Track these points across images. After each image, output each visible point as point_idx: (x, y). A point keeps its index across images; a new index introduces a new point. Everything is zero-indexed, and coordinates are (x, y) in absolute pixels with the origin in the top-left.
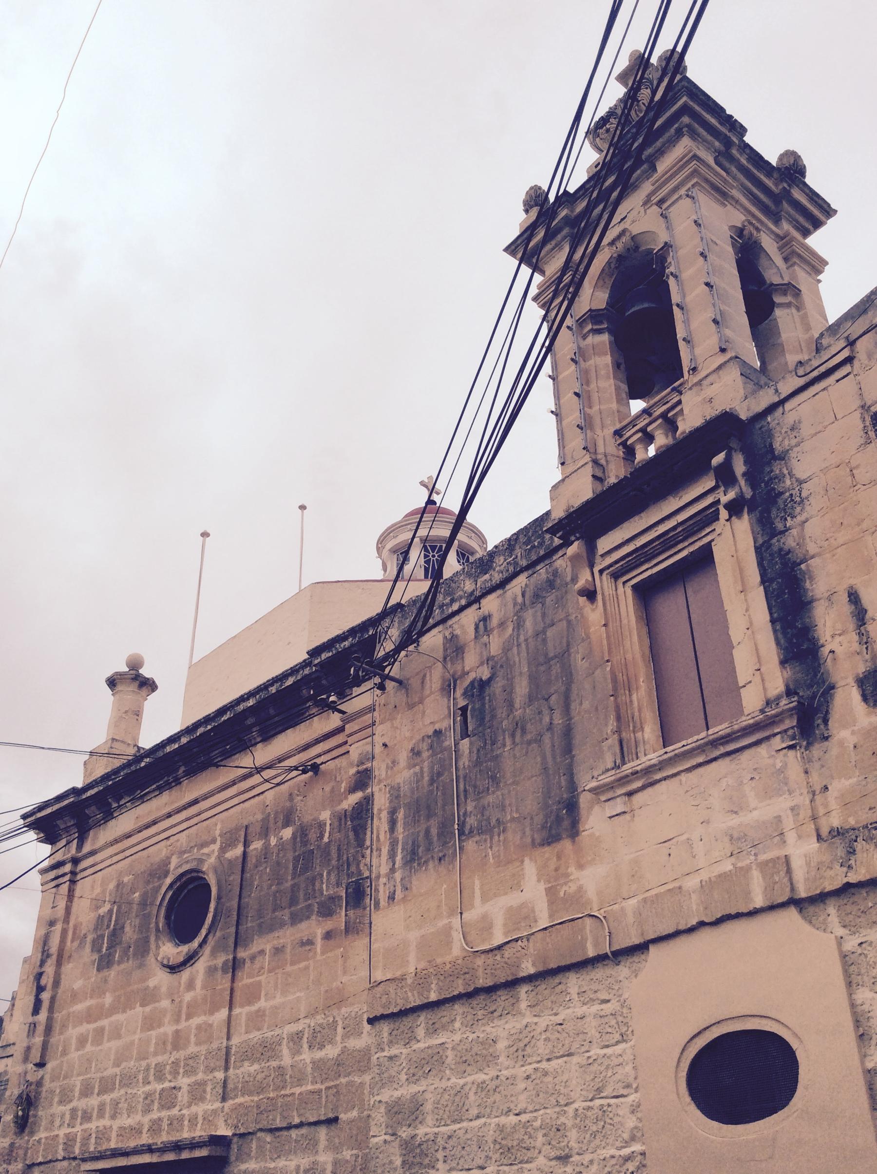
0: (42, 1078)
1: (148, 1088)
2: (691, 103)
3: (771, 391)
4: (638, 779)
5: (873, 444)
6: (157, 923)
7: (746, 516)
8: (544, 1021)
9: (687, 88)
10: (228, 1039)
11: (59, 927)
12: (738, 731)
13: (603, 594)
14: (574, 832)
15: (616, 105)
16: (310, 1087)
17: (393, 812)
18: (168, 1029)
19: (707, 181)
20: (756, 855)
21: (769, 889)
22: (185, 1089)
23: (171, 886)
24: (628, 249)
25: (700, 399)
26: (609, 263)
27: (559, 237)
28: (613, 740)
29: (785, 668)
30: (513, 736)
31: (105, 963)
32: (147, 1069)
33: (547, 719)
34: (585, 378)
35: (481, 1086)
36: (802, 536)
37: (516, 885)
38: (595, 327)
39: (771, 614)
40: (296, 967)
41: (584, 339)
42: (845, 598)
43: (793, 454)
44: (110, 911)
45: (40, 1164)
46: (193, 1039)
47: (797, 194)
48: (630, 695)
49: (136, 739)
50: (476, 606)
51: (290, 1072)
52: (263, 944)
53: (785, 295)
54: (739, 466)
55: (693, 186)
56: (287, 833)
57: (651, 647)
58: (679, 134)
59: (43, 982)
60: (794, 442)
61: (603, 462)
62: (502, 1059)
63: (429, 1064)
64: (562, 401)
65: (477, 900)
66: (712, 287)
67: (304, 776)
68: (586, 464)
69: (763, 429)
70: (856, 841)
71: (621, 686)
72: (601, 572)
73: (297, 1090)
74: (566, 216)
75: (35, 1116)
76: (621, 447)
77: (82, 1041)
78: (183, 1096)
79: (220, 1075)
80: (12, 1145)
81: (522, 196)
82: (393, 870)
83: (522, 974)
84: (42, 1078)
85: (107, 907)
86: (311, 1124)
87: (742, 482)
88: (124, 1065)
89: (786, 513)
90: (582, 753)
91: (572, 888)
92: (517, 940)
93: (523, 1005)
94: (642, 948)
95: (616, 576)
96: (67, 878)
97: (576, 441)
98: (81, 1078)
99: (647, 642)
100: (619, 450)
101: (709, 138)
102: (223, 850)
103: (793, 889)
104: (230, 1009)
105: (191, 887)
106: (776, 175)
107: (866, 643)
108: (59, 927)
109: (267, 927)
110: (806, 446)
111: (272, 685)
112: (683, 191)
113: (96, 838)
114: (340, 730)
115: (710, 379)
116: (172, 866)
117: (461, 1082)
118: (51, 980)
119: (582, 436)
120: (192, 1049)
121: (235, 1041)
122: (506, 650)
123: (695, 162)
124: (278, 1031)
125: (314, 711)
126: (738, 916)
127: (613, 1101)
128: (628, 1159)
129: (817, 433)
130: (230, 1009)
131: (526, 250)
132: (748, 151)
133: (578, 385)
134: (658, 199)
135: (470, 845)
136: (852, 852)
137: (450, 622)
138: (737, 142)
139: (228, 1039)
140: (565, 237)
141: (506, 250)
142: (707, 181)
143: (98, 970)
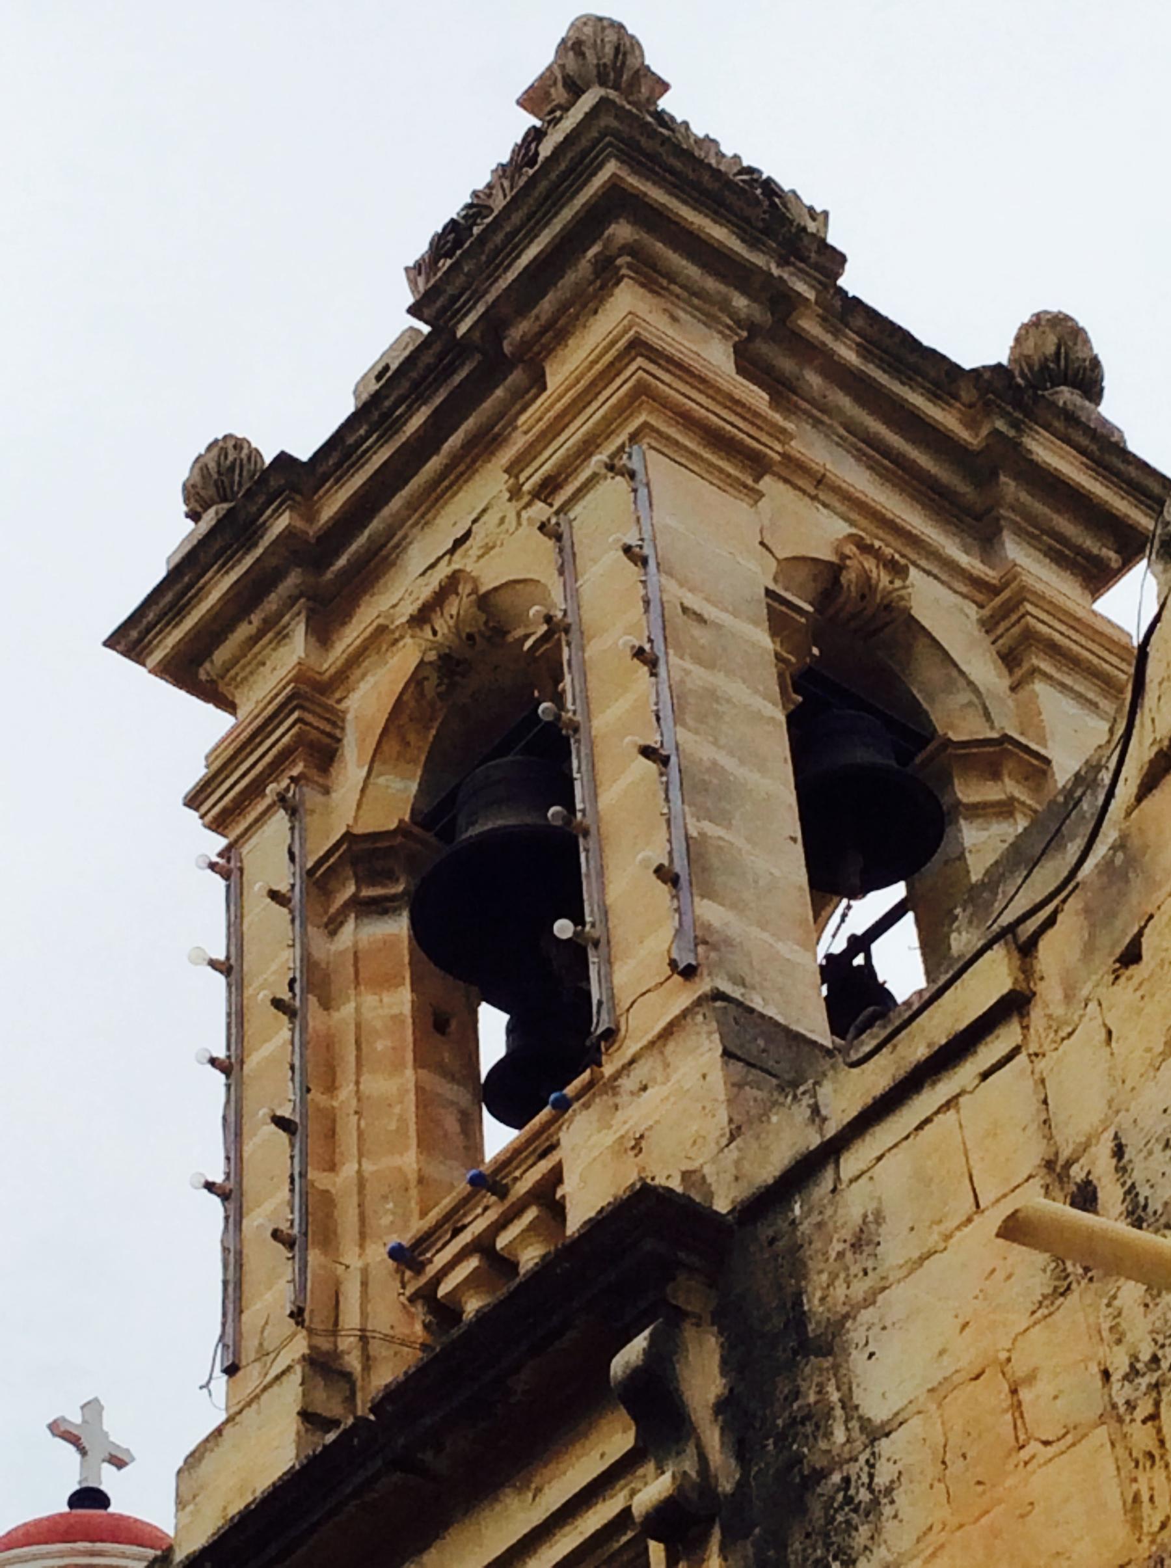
2: (633, 180)
3: (802, 1112)
5: (1073, 1298)
9: (615, 134)
15: (490, 186)
19: (687, 420)
24: (470, 637)
25: (608, 1138)
26: (416, 680)
27: (272, 602)
34: (317, 1067)
38: (368, 892)
41: (333, 933)
43: (856, 1333)
47: (1048, 452)
53: (996, 776)
54: (703, 1380)
55: (634, 438)
58: (606, 276)
60: (860, 1288)
61: (353, 1362)
64: (248, 1149)
66: (665, 761)
68: (289, 1368)
74: (289, 534)
76: (419, 1309)
81: (182, 471)
87: (712, 1437)
89: (827, 1546)
97: (272, 1295)
100: (412, 1316)
101: (711, 284)
106: (968, 394)
110: (897, 1299)
112: (600, 458)
115: (640, 1072)
119: (288, 1271)
123: (640, 361)
129: (923, 1259)
131: (174, 636)
132: (859, 322)
133: (291, 1091)
134: (537, 478)
138: (811, 295)
140: (292, 600)
142: (687, 420)
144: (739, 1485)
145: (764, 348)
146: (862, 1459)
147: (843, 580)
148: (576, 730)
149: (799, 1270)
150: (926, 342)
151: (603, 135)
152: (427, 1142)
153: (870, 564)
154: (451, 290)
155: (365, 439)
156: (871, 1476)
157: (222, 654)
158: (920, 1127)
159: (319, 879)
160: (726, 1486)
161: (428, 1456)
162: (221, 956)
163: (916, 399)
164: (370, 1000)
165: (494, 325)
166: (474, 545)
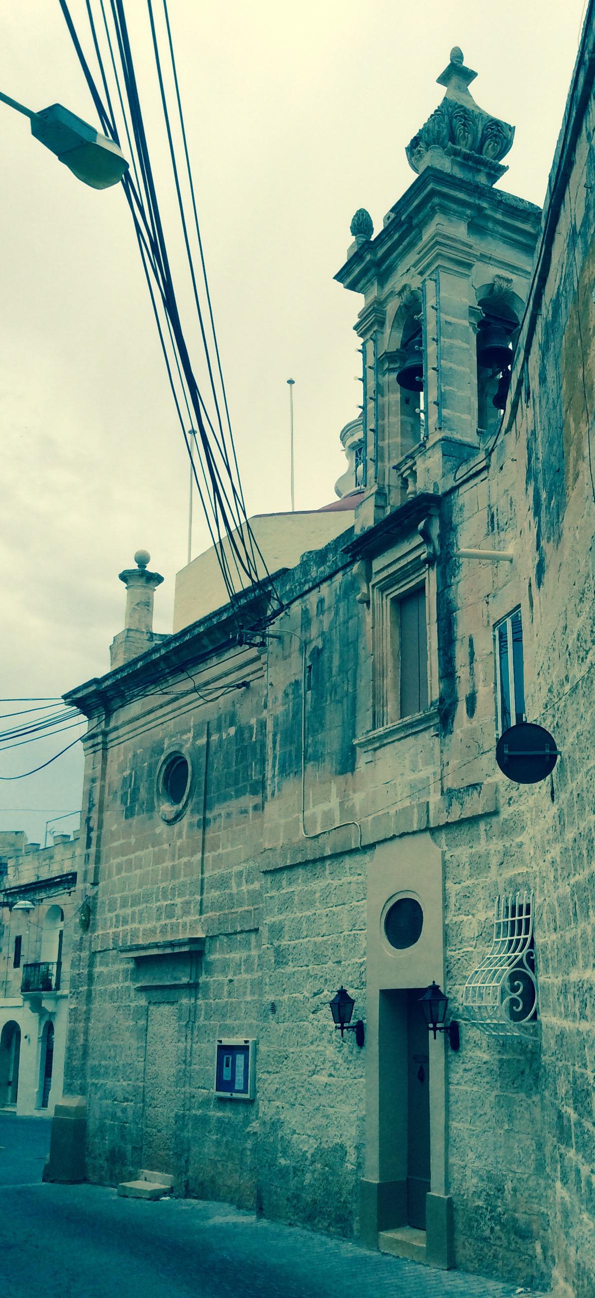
0: (97, 894)
1: (159, 904)
4: (377, 742)
6: (158, 789)
8: (336, 883)
10: (202, 873)
11: (98, 784)
13: (373, 604)
14: (353, 770)
16: (246, 908)
17: (275, 735)
18: (168, 864)
19: (451, 260)
21: (420, 820)
22: (179, 906)
23: (164, 762)
27: (369, 275)
28: (370, 713)
30: (331, 695)
31: (130, 813)
32: (157, 893)
33: (346, 688)
34: (380, 414)
35: (308, 918)
37: (327, 799)
40: (239, 827)
43: (459, 529)
44: (131, 775)
45: (100, 952)
46: (182, 873)
49: (149, 626)
50: (317, 589)
51: (236, 896)
52: (220, 809)
54: (435, 531)
56: (232, 731)
57: (401, 644)
58: (433, 211)
59: (91, 825)
60: (460, 519)
62: (317, 904)
63: (286, 904)
65: (311, 806)
67: (238, 690)
71: (377, 674)
72: (373, 586)
73: (240, 909)
75: (94, 919)
77: (119, 870)
78: (178, 911)
79: (198, 898)
80: (82, 938)
81: (350, 224)
82: (274, 775)
83: (326, 854)
84: (97, 894)
85: (127, 773)
86: (246, 932)
87: (436, 543)
88: (144, 887)
90: (359, 717)
91: (349, 804)
92: (324, 833)
93: (327, 872)
94: (372, 846)
95: (382, 590)
96: (100, 746)
98: (120, 895)
101: (460, 209)
102: (195, 738)
103: (428, 821)
104: (203, 854)
105: (178, 762)
108: (98, 784)
109: (225, 798)
110: (465, 523)
111: (214, 617)
113: (117, 717)
114: (257, 659)
116: (165, 746)
117: (300, 915)
118: (96, 824)
120: (182, 879)
121: (206, 875)
122: (331, 629)
124: (229, 870)
126: (408, 834)
127: (359, 932)
128: (362, 964)
130: (203, 854)
135: (309, 766)
137: (306, 597)
139: (202, 873)
140: (373, 276)
141: (340, 277)
142: (451, 260)
143: (126, 818)
145: (476, 221)
149: (452, 512)
152: (403, 435)
153: (501, 282)
159: (380, 361)
160: (438, 553)
164: (392, 396)
165: (410, 218)
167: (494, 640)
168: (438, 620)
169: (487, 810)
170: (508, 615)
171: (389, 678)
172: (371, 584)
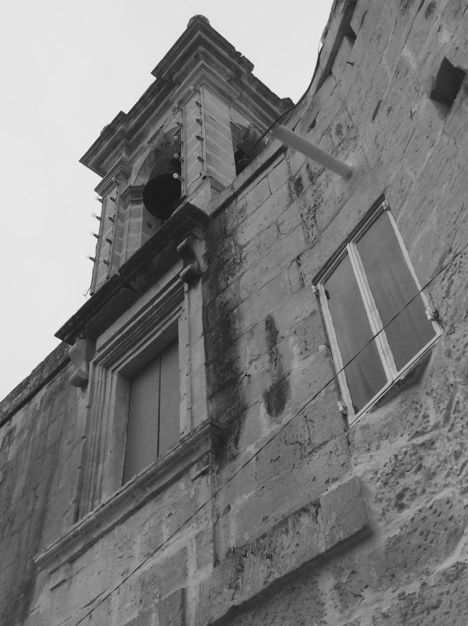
5: (295, 203)
7: (200, 285)
12: (162, 467)
13: (93, 382)
20: (160, 597)
24: (162, 144)
26: (149, 157)
27: (118, 147)
29: (211, 402)
34: (119, 232)
36: (238, 288)
39: (207, 357)
42: (262, 326)
48: (97, 466)
54: (200, 249)
58: (197, 58)
66: (202, 140)
69: (221, 219)
70: (245, 556)
71: (90, 458)
74: (122, 131)
95: (107, 367)
99: (124, 420)
106: (281, 104)
107: (275, 360)
110: (249, 221)
125: (211, 408)
132: (256, 82)
136: (240, 570)
140: (123, 146)
144: (208, 270)
146: (238, 254)
147: (250, 132)
148: (183, 143)
150: (272, 91)
151: (197, 25)
153: (256, 130)
154: (161, 67)
155: (140, 108)
156: (240, 256)
157: (106, 161)
158: (258, 184)
159: (123, 197)
161: (132, 283)
162: (100, 216)
163: (270, 104)
165: (171, 74)
166: (164, 127)
167: (318, 297)
168: (205, 333)
169: (341, 535)
170: (347, 241)
171: (107, 461)
172: (91, 364)
